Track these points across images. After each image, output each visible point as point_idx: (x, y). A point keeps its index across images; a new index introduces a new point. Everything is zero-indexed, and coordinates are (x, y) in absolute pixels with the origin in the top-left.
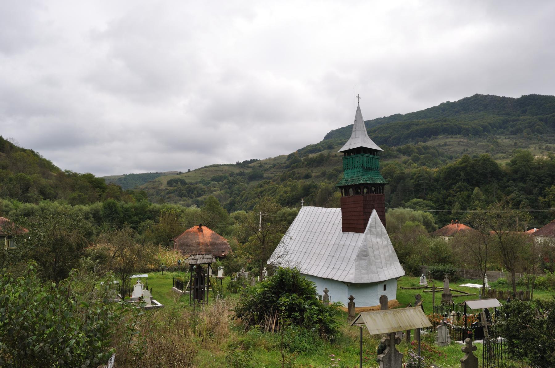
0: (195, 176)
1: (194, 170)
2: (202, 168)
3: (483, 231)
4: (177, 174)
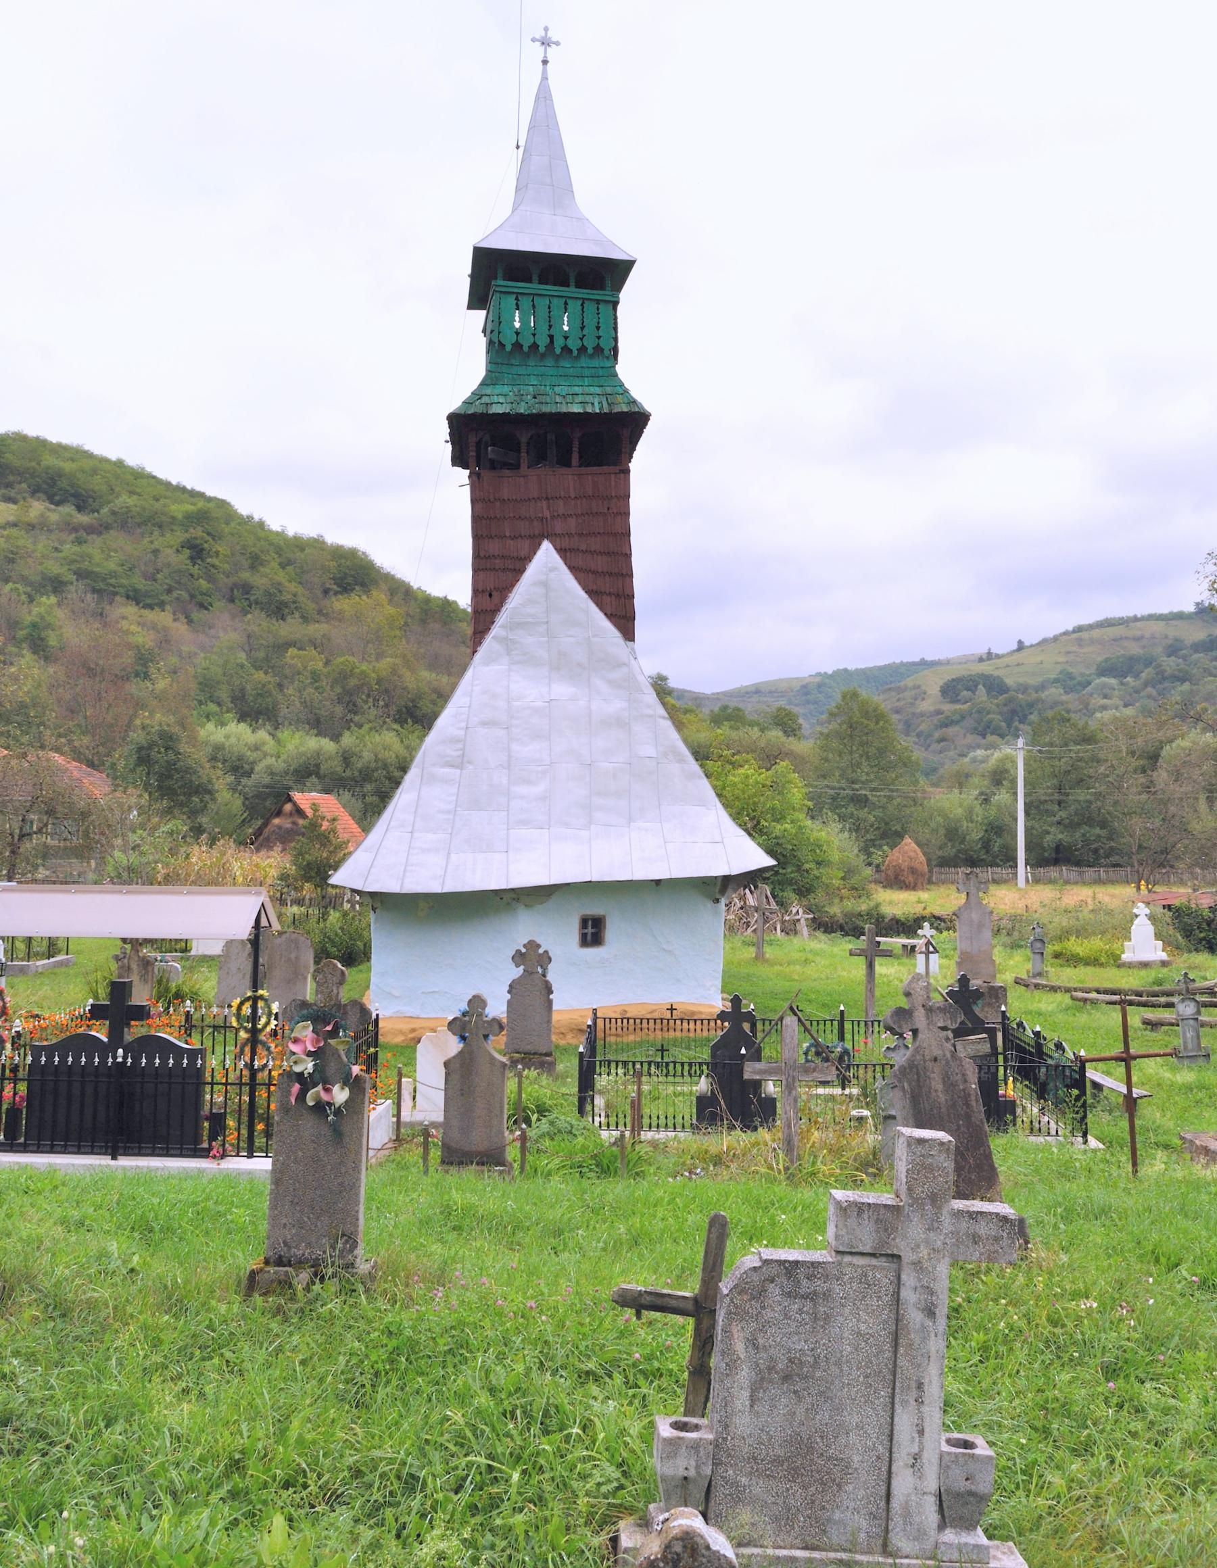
2: (1066, 633)
4: (981, 660)
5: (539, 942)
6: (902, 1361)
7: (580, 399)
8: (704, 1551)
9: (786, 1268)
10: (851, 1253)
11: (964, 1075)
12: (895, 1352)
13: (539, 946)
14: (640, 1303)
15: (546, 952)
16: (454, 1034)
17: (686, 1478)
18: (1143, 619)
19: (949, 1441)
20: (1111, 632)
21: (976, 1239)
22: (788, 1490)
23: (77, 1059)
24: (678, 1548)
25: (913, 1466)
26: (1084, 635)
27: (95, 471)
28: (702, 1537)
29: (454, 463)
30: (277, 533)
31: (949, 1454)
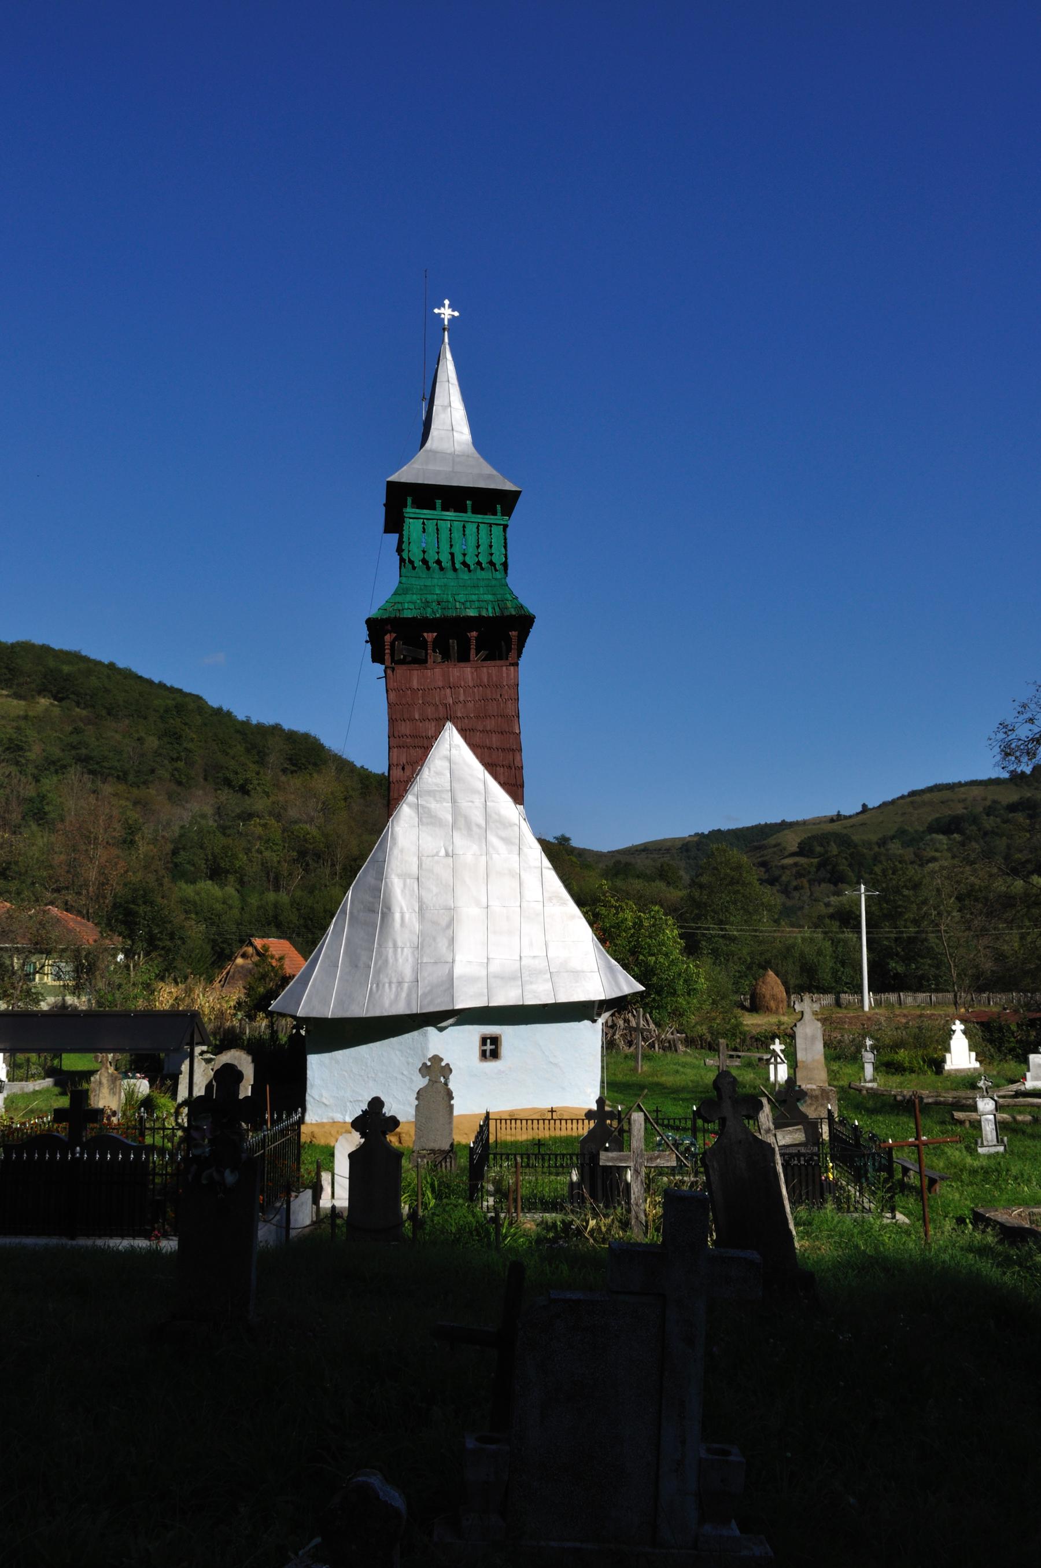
2: (903, 797)
4: (832, 820)
13: (441, 1060)
15: (448, 1065)
20: (947, 794)
26: (917, 798)
29: (373, 661)
30: (243, 723)
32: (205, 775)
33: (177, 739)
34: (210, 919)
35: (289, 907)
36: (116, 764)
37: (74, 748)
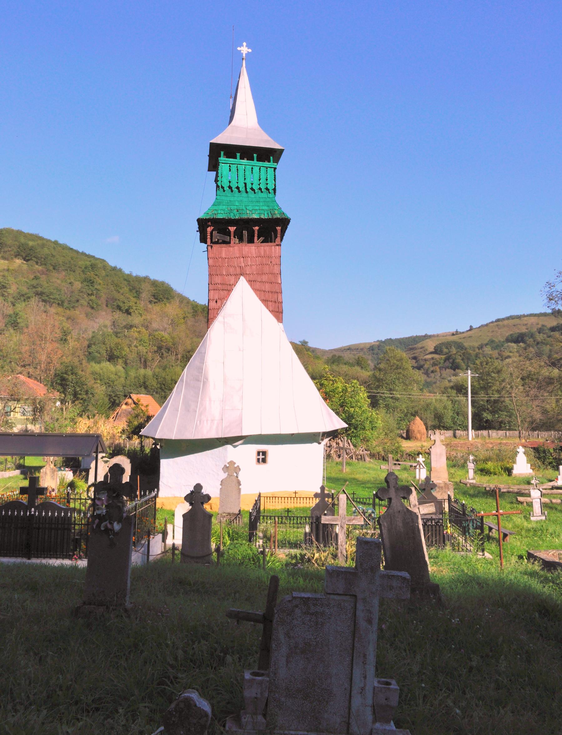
0: (481, 336)
1: (479, 327)
2: (492, 322)
3: (453, 587)
4: (453, 334)
5: (235, 461)
6: (356, 645)
7: (258, 211)
8: (194, 708)
9: (303, 601)
10: (333, 594)
11: (412, 519)
12: (354, 640)
13: (235, 463)
14: (239, 617)
15: (238, 466)
16: (187, 502)
17: (256, 698)
18: (528, 316)
19: (379, 682)
20: (511, 322)
21: (391, 588)
22: (303, 704)
23: (13, 513)
24: (182, 705)
25: (361, 693)
27: (43, 246)
28: (194, 701)
31: (378, 687)
32: (107, 304)
33: (91, 283)
34: (108, 383)
35: (152, 377)
36: (57, 296)
37: (34, 287)
